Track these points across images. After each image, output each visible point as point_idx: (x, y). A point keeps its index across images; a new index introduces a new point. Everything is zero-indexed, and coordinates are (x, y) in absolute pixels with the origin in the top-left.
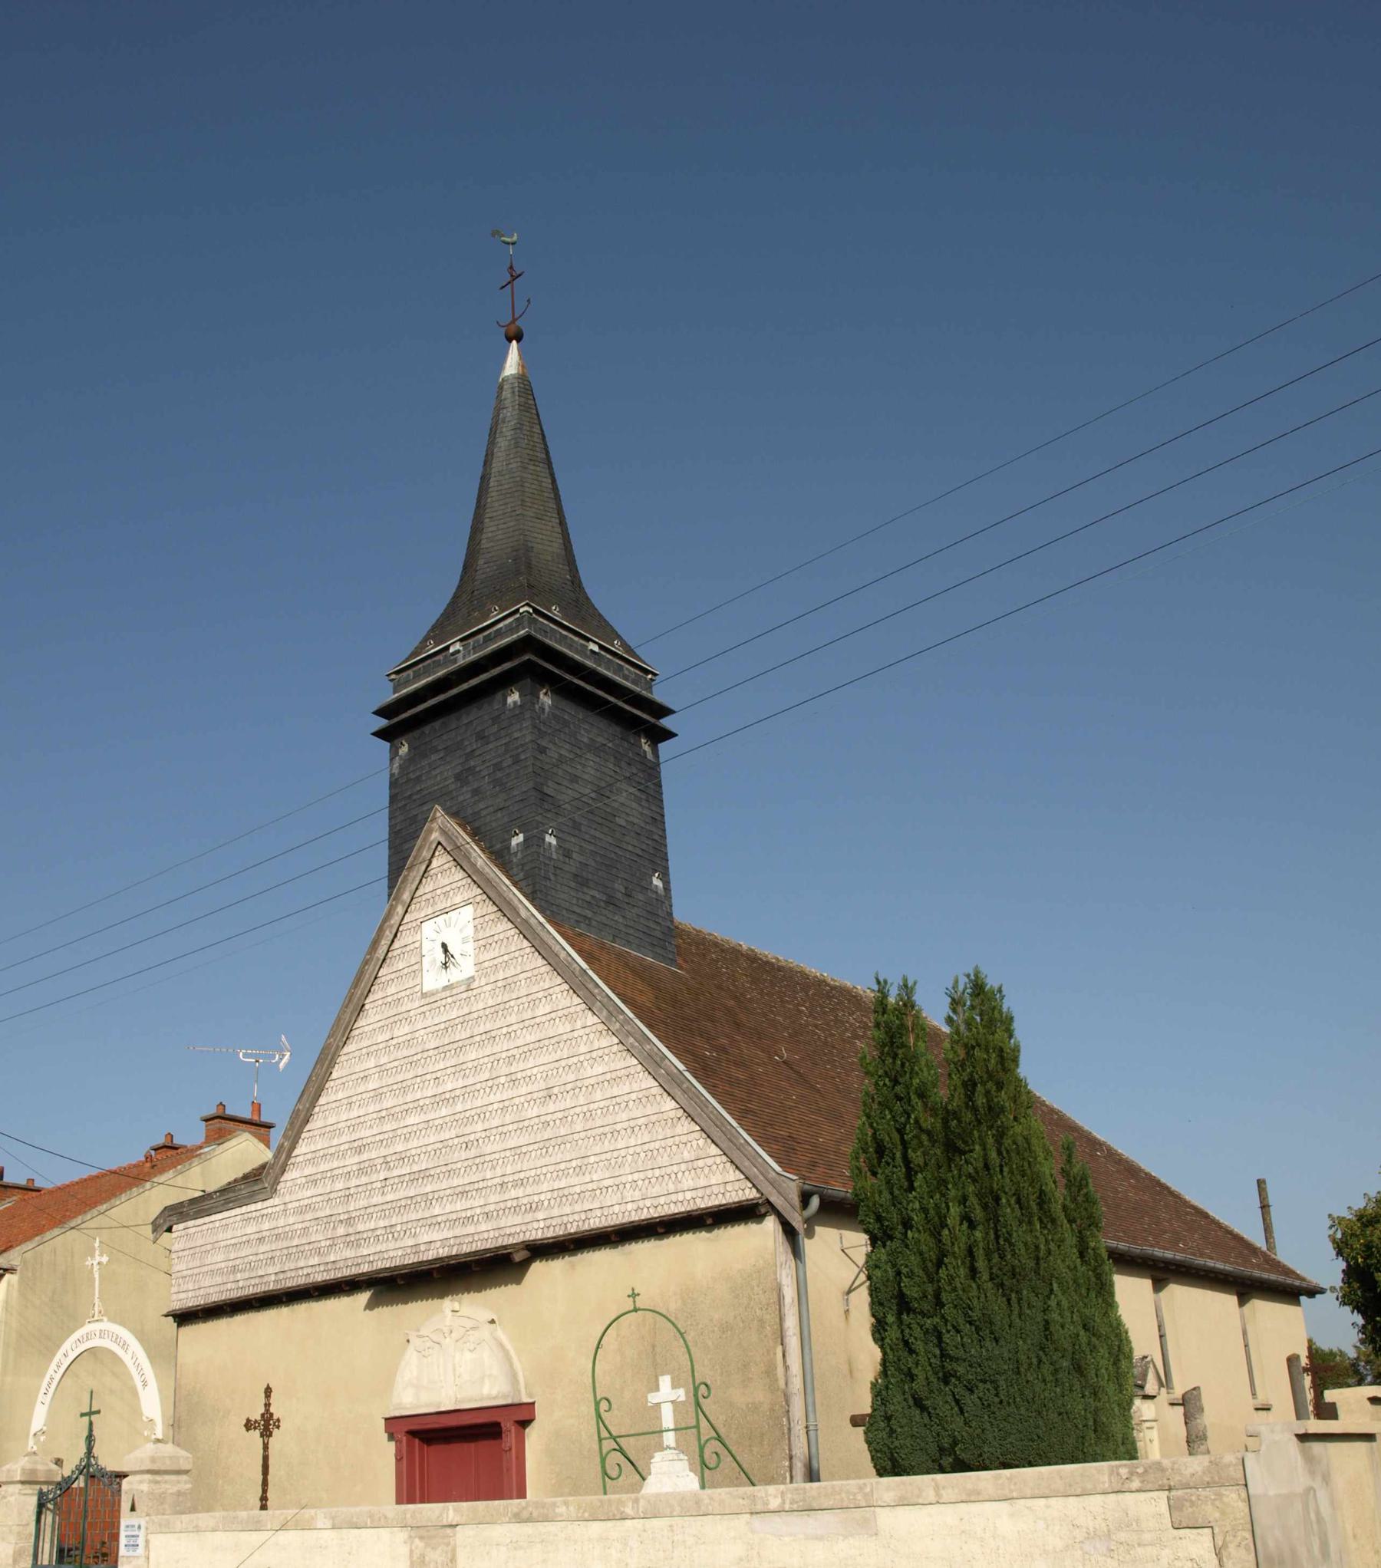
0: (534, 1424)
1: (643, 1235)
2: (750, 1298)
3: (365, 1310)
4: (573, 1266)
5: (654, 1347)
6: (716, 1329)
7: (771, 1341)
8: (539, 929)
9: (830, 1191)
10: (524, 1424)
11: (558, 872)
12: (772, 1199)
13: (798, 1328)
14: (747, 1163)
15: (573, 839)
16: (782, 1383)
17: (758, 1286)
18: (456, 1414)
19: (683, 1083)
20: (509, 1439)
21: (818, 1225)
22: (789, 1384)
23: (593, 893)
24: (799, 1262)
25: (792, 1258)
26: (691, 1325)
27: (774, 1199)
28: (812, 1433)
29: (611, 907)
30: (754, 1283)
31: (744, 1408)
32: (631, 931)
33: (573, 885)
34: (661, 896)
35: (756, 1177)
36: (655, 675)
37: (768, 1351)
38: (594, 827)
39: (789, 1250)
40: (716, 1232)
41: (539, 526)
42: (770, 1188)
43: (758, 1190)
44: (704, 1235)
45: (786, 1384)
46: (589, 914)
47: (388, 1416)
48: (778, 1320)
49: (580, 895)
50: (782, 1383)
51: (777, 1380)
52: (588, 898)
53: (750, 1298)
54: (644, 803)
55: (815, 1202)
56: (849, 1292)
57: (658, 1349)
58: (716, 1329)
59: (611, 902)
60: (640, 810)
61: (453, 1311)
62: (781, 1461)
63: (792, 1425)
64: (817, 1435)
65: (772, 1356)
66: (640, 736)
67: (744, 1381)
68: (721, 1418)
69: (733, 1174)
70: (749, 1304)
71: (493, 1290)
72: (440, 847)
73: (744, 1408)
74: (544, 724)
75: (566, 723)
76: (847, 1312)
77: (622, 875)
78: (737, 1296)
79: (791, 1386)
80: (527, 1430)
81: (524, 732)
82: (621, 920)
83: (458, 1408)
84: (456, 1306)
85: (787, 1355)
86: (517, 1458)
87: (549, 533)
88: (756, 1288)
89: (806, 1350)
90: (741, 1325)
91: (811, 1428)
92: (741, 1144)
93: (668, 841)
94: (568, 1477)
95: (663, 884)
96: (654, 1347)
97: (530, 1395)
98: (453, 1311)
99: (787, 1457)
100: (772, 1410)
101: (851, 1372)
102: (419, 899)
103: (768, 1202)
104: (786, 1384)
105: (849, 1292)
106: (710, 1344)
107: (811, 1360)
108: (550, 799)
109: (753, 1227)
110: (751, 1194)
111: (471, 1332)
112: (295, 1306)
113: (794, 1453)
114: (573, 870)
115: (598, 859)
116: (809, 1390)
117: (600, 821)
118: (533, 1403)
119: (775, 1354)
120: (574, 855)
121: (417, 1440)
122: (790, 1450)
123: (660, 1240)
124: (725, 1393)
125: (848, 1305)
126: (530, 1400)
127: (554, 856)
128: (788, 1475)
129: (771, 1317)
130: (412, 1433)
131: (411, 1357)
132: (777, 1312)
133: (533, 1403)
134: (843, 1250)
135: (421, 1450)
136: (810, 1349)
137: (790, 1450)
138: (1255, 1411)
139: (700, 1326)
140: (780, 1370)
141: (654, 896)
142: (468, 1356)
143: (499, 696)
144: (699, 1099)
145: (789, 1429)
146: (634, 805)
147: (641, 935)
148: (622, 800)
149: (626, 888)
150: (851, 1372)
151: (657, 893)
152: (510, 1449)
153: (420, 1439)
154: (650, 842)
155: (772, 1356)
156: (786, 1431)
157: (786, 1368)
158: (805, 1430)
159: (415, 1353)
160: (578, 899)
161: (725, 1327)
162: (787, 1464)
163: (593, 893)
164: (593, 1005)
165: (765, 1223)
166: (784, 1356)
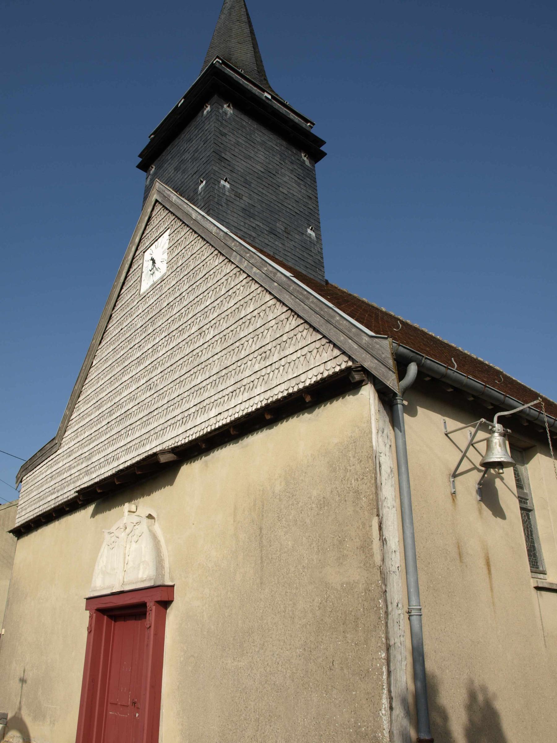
0: (174, 605)
1: (257, 427)
2: (346, 470)
3: (91, 518)
4: (206, 462)
5: (261, 529)
6: (314, 506)
7: (366, 513)
8: (202, 222)
9: (429, 362)
10: (166, 604)
11: (229, 203)
12: (366, 365)
13: (398, 500)
14: (342, 337)
15: (244, 189)
16: (377, 559)
17: (354, 457)
18: (121, 595)
19: (290, 286)
20: (152, 617)
21: (421, 407)
22: (387, 560)
23: (258, 223)
24: (397, 431)
25: (391, 428)
26: (293, 504)
27: (369, 363)
28: (415, 619)
29: (273, 236)
30: (350, 454)
31: (339, 588)
32: (289, 254)
33: (241, 214)
34: (313, 240)
35: (351, 348)
36: (314, 124)
37: (364, 524)
38: (262, 187)
39: (387, 419)
40: (317, 411)
41: (240, 46)
42: (364, 355)
43: (350, 358)
44: (306, 416)
45: (383, 560)
46: (254, 234)
47: (87, 597)
48: (373, 489)
49: (247, 221)
50: (377, 559)
51: (372, 556)
52: (254, 225)
53: (346, 470)
54: (302, 186)
55: (413, 369)
56: (455, 476)
57: (264, 532)
58: (314, 506)
59: (272, 232)
60: (300, 190)
61: (129, 511)
62: (378, 652)
63: (390, 609)
64: (420, 621)
65: (368, 528)
66: (301, 152)
67: (339, 558)
68: (317, 599)
69: (330, 352)
70: (345, 477)
71: (157, 492)
72: (158, 207)
73: (339, 588)
74: (225, 121)
75: (244, 127)
76: (454, 494)
77: (283, 220)
78: (334, 470)
79: (388, 562)
80: (168, 611)
81: (211, 124)
82: (280, 245)
83: (122, 590)
84: (133, 508)
85: (384, 527)
86: (155, 635)
87: (246, 50)
88: (352, 459)
89: (407, 524)
90: (337, 499)
91: (413, 613)
92: (337, 321)
93: (320, 208)
94: (192, 656)
95: (316, 235)
96: (261, 529)
97: (172, 579)
98: (129, 511)
99: (384, 647)
100: (367, 590)
101: (460, 555)
102: (144, 239)
103: (363, 370)
104: (383, 560)
105: (455, 476)
106: (308, 521)
107: (413, 534)
108: (227, 162)
109: (350, 399)
110: (343, 363)
111: (137, 526)
112: (62, 520)
113: (392, 643)
114: (243, 206)
115: (264, 205)
116: (411, 569)
117: (267, 185)
118: (173, 586)
119: (371, 526)
120: (244, 198)
121: (106, 617)
122: (387, 638)
123: (270, 429)
124: (321, 572)
125: (454, 488)
126: (171, 583)
127: (227, 193)
128: (384, 669)
129: (366, 488)
130: (102, 611)
131: (104, 550)
132: (373, 481)
133: (173, 586)
134: (446, 435)
135: (108, 626)
136: (412, 523)
137: (387, 638)
138: (534, 591)
139: (300, 504)
140: (376, 544)
141: (308, 239)
142: (134, 546)
143: (200, 114)
144: (302, 294)
145: (386, 613)
146: (294, 185)
147: (297, 259)
148: (285, 179)
149: (285, 228)
150: (460, 555)
151: (311, 238)
152: (150, 627)
153: (107, 616)
154: (305, 208)
155: (368, 528)
156: (382, 615)
157: (383, 541)
158: (407, 616)
159: (107, 546)
160: (245, 223)
161: (323, 503)
162: (383, 655)
163: (258, 223)
164: (231, 256)
165: (361, 392)
166: (380, 528)
